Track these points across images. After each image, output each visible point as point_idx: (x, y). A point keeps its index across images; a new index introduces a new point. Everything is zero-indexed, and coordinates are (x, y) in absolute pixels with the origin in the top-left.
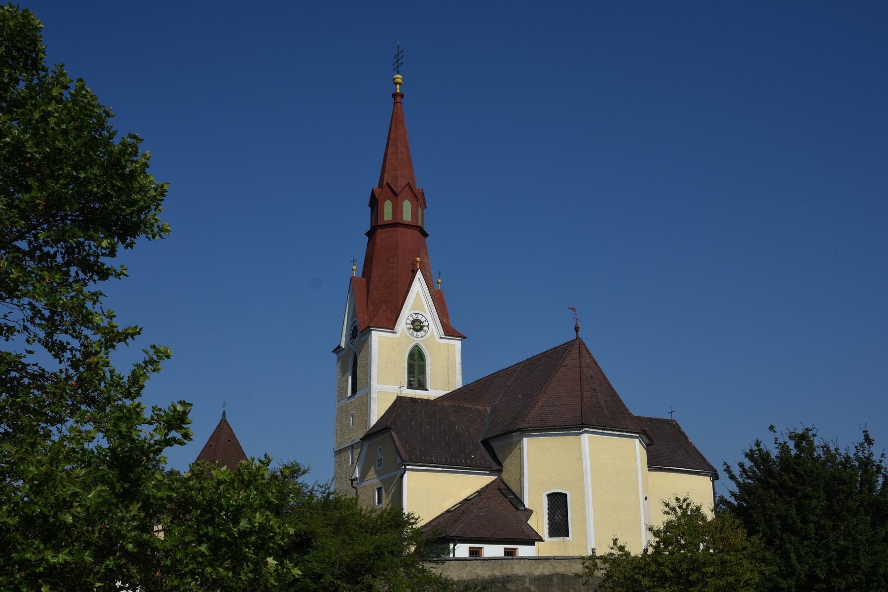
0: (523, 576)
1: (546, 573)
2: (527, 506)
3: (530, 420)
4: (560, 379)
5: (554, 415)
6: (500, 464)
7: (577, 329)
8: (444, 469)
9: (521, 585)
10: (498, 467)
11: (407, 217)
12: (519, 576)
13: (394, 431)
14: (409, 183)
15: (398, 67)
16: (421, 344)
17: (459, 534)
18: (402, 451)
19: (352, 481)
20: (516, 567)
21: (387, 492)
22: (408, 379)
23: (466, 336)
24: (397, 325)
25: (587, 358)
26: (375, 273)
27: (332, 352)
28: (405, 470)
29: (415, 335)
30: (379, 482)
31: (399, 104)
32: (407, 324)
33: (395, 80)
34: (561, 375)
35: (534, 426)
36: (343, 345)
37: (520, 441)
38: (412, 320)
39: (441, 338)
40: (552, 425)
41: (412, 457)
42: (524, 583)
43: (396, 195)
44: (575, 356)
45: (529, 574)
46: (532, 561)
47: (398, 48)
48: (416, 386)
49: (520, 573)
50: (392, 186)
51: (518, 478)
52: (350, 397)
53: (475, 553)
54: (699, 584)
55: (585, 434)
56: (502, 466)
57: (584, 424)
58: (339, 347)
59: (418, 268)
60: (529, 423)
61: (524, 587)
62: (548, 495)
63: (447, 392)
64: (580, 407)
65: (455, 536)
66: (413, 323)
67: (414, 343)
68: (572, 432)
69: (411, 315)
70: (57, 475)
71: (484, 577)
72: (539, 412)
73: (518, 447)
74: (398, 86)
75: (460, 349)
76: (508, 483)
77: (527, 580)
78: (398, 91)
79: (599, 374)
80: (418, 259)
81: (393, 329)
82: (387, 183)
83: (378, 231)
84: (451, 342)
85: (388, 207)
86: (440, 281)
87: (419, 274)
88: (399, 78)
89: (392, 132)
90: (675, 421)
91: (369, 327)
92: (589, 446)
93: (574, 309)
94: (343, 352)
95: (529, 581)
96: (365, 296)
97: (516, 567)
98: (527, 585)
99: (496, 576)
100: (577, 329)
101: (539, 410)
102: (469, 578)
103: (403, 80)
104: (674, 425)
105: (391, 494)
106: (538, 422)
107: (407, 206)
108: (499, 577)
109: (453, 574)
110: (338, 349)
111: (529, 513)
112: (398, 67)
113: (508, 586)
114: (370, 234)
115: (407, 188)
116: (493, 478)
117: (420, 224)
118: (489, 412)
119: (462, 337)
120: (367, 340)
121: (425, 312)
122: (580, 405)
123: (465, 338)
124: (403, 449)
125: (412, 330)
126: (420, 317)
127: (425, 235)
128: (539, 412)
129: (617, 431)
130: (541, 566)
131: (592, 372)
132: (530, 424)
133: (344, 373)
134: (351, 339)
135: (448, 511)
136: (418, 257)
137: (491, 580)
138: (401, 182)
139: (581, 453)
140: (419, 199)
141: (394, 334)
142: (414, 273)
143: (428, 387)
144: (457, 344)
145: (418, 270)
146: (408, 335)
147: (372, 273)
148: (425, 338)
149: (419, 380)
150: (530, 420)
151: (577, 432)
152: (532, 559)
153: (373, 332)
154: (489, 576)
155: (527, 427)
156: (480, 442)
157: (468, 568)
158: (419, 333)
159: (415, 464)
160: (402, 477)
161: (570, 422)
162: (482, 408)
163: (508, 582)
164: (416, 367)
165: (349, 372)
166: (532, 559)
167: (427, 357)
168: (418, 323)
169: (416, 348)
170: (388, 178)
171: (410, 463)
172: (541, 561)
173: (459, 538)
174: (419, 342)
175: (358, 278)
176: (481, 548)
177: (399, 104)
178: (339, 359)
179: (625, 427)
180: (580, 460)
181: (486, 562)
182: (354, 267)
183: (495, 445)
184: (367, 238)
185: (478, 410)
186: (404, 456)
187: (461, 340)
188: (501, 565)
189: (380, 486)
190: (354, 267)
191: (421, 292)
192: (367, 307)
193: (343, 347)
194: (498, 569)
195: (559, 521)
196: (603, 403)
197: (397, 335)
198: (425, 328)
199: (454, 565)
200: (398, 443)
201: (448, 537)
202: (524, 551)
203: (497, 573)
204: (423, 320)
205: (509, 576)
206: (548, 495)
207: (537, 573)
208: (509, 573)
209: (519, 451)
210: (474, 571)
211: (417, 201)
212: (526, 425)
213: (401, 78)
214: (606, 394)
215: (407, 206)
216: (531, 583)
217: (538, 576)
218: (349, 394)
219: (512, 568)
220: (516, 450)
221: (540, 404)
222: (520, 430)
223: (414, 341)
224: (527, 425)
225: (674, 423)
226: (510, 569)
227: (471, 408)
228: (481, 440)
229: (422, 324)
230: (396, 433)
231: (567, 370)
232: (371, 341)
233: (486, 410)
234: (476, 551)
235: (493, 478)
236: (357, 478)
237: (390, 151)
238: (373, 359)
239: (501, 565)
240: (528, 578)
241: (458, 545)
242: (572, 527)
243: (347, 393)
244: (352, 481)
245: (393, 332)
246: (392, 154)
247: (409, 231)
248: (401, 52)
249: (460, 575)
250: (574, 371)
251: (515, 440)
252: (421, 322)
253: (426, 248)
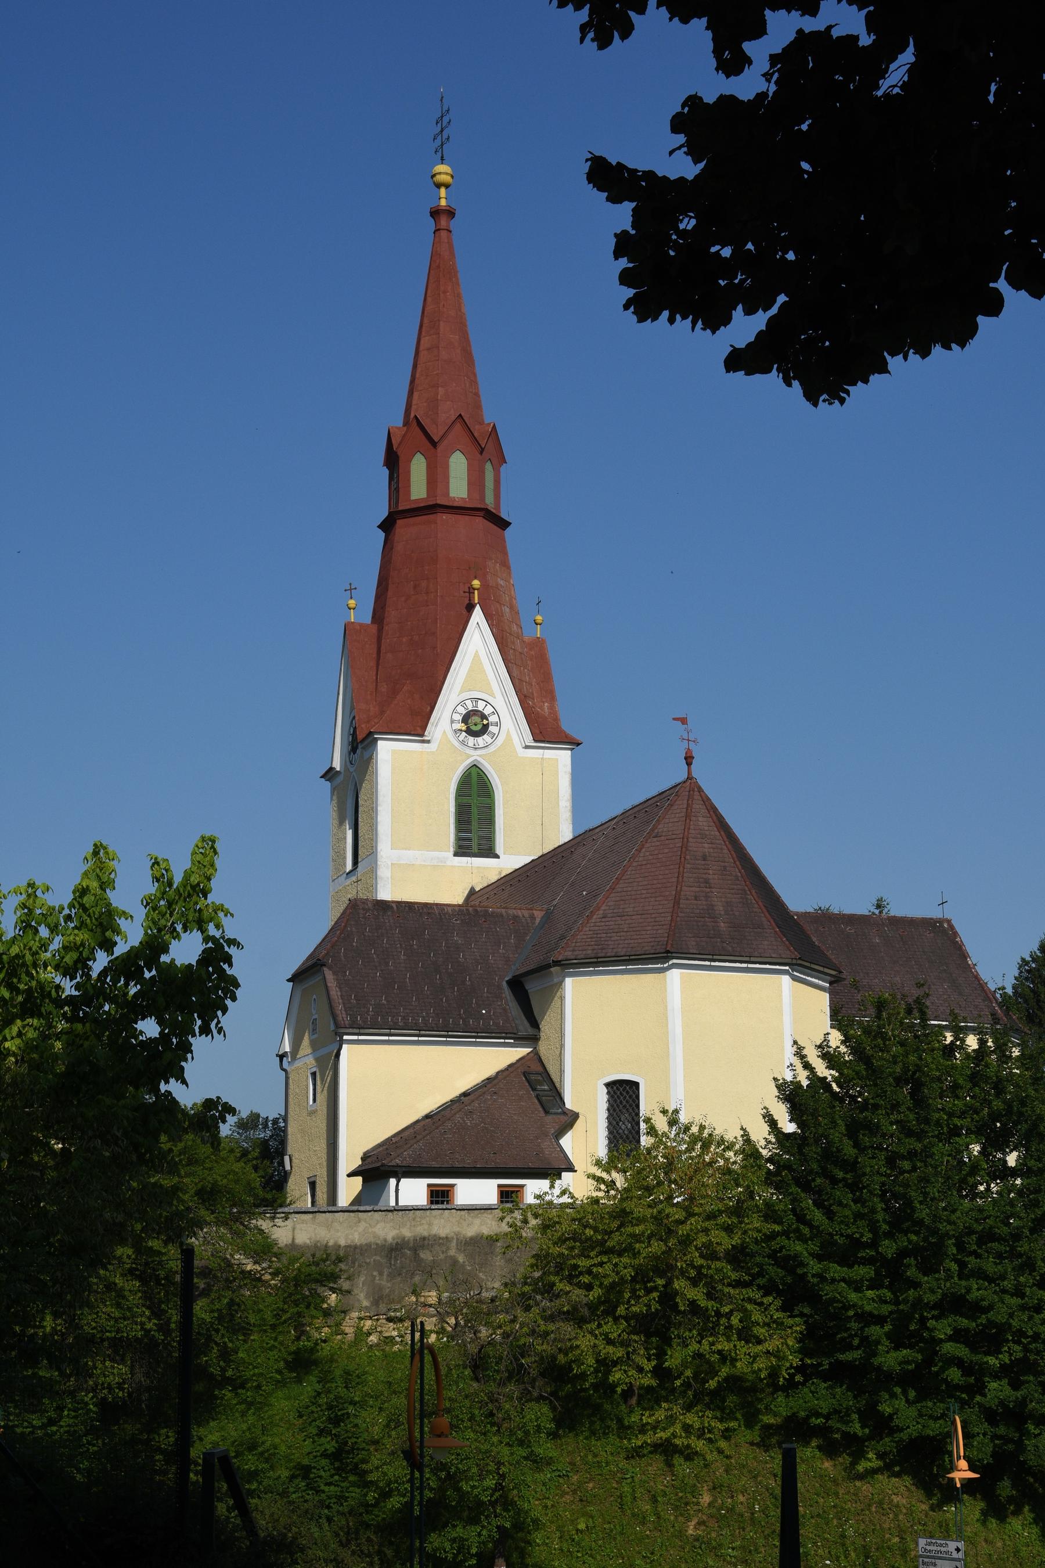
0: (447, 1238)
1: (486, 1231)
2: (569, 1105)
3: (578, 944)
4: (644, 863)
5: (622, 934)
6: (535, 1024)
7: (689, 759)
8: (420, 1039)
9: (443, 1253)
10: (531, 1031)
11: (458, 489)
12: (440, 1238)
13: (330, 968)
14: (460, 415)
15: (442, 145)
16: (482, 761)
17: (408, 1162)
18: (340, 1008)
19: (281, 1057)
20: (436, 1222)
21: (322, 1080)
22: (456, 835)
23: (579, 737)
24: (429, 725)
25: (700, 819)
26: (392, 615)
27: (321, 777)
28: (341, 1042)
29: (471, 744)
30: (314, 1062)
31: (444, 234)
32: (452, 722)
33: (435, 179)
34: (648, 854)
35: (582, 956)
36: (337, 765)
37: (561, 983)
38: (464, 712)
39: (527, 747)
40: (613, 954)
41: (357, 1018)
42: (448, 1249)
43: (434, 444)
44: (677, 815)
45: (457, 1234)
46: (463, 1213)
47: (441, 100)
48: (475, 850)
49: (443, 1232)
51: (558, 1053)
52: (351, 872)
53: (440, 1197)
55: (674, 970)
56: (539, 1029)
57: (668, 952)
58: (331, 769)
59: (476, 601)
60: (573, 951)
61: (446, 1257)
62: (608, 1085)
63: (527, 859)
64: (669, 918)
65: (398, 1166)
66: (466, 719)
67: (468, 762)
68: (650, 966)
69: (462, 703)
71: (385, 1240)
72: (597, 928)
73: (558, 994)
74: (443, 191)
75: (569, 768)
76: (545, 1062)
77: (454, 1244)
79: (722, 849)
80: (476, 583)
81: (422, 735)
82: (416, 416)
83: (399, 522)
84: (549, 754)
85: (418, 468)
86: (539, 618)
87: (478, 615)
89: (429, 299)
90: (949, 922)
91: (370, 733)
92: (682, 992)
93: (684, 721)
94: (339, 779)
95: (457, 1245)
96: (373, 664)
97: (436, 1222)
98: (452, 1252)
99: (404, 1238)
100: (689, 759)
101: (598, 924)
102: (364, 1241)
103: (452, 177)
104: (944, 930)
105: (327, 1085)
106: (590, 948)
107: (458, 465)
108: (409, 1240)
109: (339, 1234)
110: (330, 774)
111: (570, 1119)
112: (442, 145)
113: (422, 1255)
114: (387, 526)
115: (458, 426)
116: (523, 1051)
117: (489, 501)
118: (538, 921)
119: (574, 743)
120: (371, 758)
121: (493, 695)
122: (670, 914)
124: (344, 1003)
125: (464, 734)
126: (481, 706)
127: (504, 524)
128: (597, 928)
129: (741, 962)
130: (477, 1222)
131: (706, 845)
132: (576, 953)
133: (341, 822)
134: (350, 754)
135: (427, 1117)
136: (476, 578)
137: (397, 1244)
138: (447, 413)
139: (666, 1006)
141: (426, 745)
142: (470, 608)
143: (499, 850)
144: (562, 758)
145: (476, 604)
146: (456, 744)
147: (386, 615)
148: (492, 749)
149: (480, 838)
150: (578, 944)
151: (659, 966)
152: (464, 1210)
153: (380, 743)
154: (393, 1239)
155: (569, 957)
156: (504, 984)
157: (363, 1225)
158: (480, 740)
159: (362, 1031)
160: (338, 1055)
161: (647, 948)
162: (526, 913)
163: (423, 1247)
164: (474, 810)
165: (347, 822)
166: (464, 1210)
167: (497, 788)
168: (476, 719)
169: (474, 770)
170: (416, 411)
171: (351, 1030)
172: (478, 1211)
173: (404, 1169)
174: (479, 759)
175: (361, 625)
176: (453, 1186)
177: (444, 234)
178: (333, 790)
179: (756, 954)
180: (663, 1019)
181: (391, 1214)
182: (352, 603)
183: (532, 987)
184: (384, 534)
185: (515, 918)
186: (343, 1017)
187: (572, 749)
188: (414, 1219)
189: (314, 1070)
190: (352, 603)
191: (483, 653)
192: (377, 685)
193: (338, 769)
194: (408, 1226)
195: (626, 1132)
196: (721, 908)
197: (432, 747)
198: (491, 728)
199: (341, 1220)
200: (335, 993)
201: (382, 1168)
202: (533, 1189)
203: (407, 1233)
204: (488, 711)
205: (424, 1239)
206: (608, 1085)
207: (470, 1232)
208: (426, 1234)
209: (559, 1000)
210: (370, 1230)
211: (481, 453)
212: (568, 954)
213: (447, 174)
214: (733, 889)
215: (458, 465)
216: (458, 1250)
217: (471, 1238)
218: (349, 866)
219: (430, 1224)
220: (556, 1003)
221: (601, 912)
222: (557, 963)
223: (469, 756)
224: (570, 953)
225: (946, 925)
226: (426, 1227)
227: (502, 915)
228: (507, 979)
229: (485, 722)
230: (334, 973)
231: (658, 843)
232: (377, 762)
233: (533, 917)
234: (443, 1192)
235: (523, 1051)
236: (286, 1052)
237: (425, 342)
238: (380, 798)
239: (414, 1219)
240: (455, 1241)
241: (403, 1180)
243: (345, 864)
244: (281, 1057)
245: (423, 742)
246: (428, 349)
247: (463, 520)
248: (448, 111)
249: (350, 1237)
250: (671, 846)
251: (556, 980)
252: (484, 717)
253: (504, 552)
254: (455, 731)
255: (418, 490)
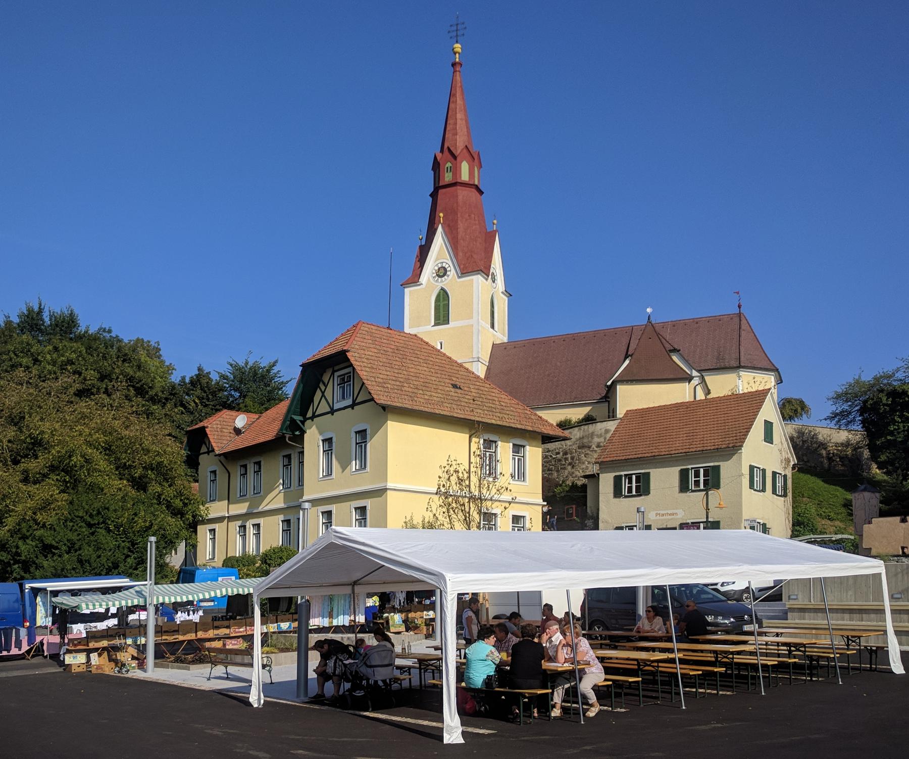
7: (739, 307)
11: (465, 176)
50: (451, 149)
54: (268, 688)
70: (156, 395)
78: (457, 60)
88: (458, 47)
93: (738, 293)
100: (739, 307)
114: (434, 195)
117: (476, 183)
123: (511, 295)
126: (444, 265)
140: (474, 158)
176: (718, 467)
242: (504, 311)
252: (439, 269)
254: (434, 277)
255: (448, 177)
